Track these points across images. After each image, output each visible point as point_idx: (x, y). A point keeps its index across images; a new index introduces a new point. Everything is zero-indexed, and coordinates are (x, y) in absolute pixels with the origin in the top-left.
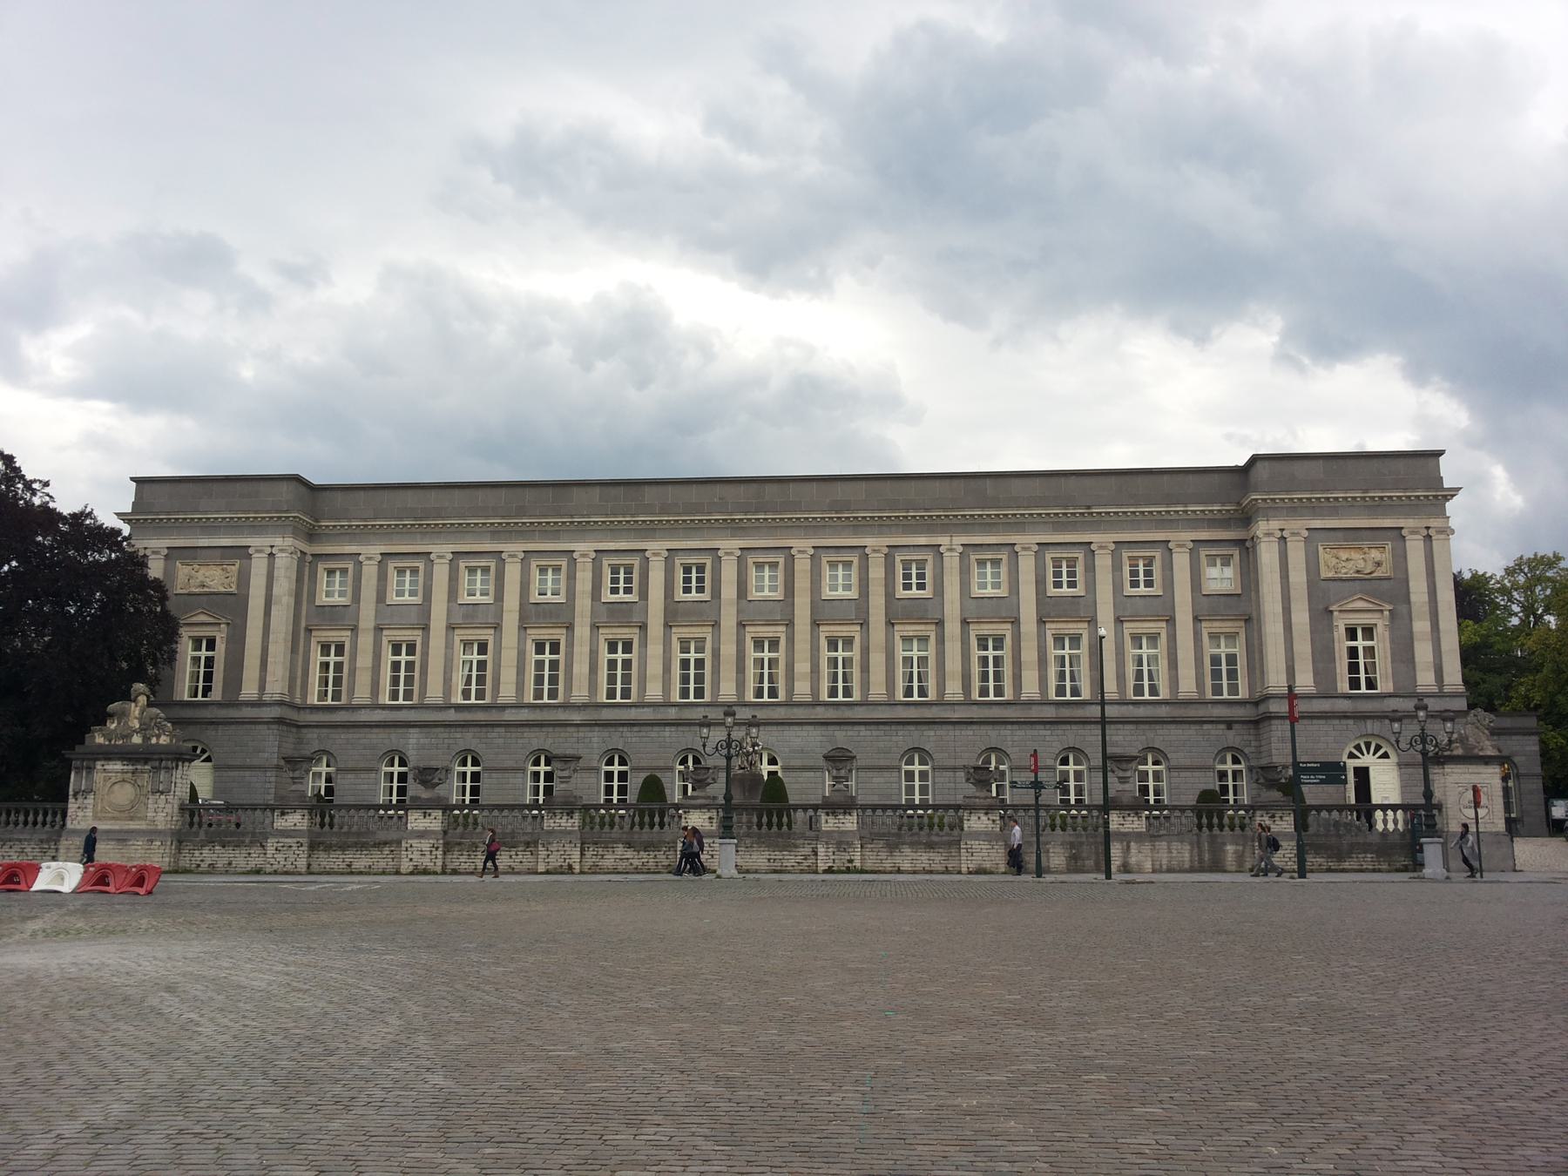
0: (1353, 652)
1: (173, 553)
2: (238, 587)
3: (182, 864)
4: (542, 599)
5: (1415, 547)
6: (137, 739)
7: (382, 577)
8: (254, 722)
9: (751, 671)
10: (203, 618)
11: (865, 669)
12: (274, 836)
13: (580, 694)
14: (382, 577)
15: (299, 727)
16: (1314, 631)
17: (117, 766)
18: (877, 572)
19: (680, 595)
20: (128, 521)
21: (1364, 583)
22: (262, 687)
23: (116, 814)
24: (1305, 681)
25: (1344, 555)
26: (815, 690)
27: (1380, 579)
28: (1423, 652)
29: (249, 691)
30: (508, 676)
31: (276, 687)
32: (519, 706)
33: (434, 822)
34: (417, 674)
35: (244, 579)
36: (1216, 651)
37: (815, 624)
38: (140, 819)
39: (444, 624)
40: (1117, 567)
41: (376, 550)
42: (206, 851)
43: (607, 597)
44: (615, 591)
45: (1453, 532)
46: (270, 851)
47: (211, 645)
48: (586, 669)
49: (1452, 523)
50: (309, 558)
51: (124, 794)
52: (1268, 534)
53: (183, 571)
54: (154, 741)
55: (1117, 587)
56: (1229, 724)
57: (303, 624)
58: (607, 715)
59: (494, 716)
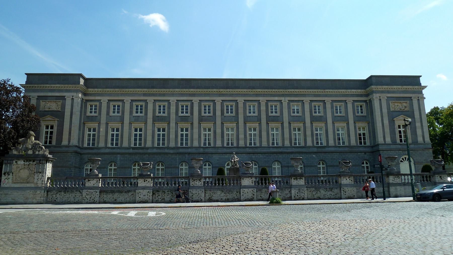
0: (400, 132)
1: (39, 98)
2: (61, 108)
3: (48, 200)
4: (160, 115)
5: (415, 102)
6: (30, 152)
7: (108, 107)
8: (67, 152)
9: (203, 138)
10: (49, 119)
11: (260, 136)
12: (86, 189)
13: (172, 144)
14: (108, 107)
15: (81, 154)
16: (390, 126)
17: (21, 162)
18: (263, 108)
19: (203, 114)
20: (24, 87)
21: (401, 112)
22: (69, 141)
23: (22, 181)
24: (388, 140)
25: (396, 104)
26: (246, 143)
27: (406, 111)
28: (419, 132)
29: (65, 142)
30: (149, 138)
31: (74, 141)
32: (153, 148)
33: (150, 183)
34: (119, 138)
35: (63, 106)
36: (360, 132)
37: (245, 123)
38: (32, 183)
39: (129, 122)
40: (332, 107)
41: (106, 99)
42: (58, 195)
43: (180, 114)
44: (182, 113)
45: (425, 98)
46: (84, 195)
47: (52, 127)
48: (174, 136)
49: (424, 96)
50: (85, 101)
51: (24, 173)
52: (377, 98)
53: (42, 103)
54: (37, 153)
55: (333, 113)
56: (365, 153)
57: (82, 122)
58: (181, 151)
59: (145, 151)
